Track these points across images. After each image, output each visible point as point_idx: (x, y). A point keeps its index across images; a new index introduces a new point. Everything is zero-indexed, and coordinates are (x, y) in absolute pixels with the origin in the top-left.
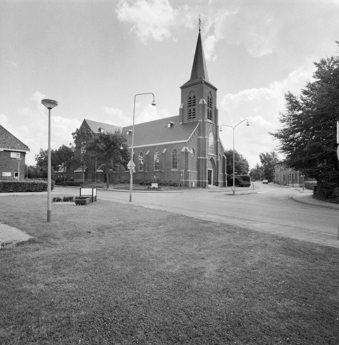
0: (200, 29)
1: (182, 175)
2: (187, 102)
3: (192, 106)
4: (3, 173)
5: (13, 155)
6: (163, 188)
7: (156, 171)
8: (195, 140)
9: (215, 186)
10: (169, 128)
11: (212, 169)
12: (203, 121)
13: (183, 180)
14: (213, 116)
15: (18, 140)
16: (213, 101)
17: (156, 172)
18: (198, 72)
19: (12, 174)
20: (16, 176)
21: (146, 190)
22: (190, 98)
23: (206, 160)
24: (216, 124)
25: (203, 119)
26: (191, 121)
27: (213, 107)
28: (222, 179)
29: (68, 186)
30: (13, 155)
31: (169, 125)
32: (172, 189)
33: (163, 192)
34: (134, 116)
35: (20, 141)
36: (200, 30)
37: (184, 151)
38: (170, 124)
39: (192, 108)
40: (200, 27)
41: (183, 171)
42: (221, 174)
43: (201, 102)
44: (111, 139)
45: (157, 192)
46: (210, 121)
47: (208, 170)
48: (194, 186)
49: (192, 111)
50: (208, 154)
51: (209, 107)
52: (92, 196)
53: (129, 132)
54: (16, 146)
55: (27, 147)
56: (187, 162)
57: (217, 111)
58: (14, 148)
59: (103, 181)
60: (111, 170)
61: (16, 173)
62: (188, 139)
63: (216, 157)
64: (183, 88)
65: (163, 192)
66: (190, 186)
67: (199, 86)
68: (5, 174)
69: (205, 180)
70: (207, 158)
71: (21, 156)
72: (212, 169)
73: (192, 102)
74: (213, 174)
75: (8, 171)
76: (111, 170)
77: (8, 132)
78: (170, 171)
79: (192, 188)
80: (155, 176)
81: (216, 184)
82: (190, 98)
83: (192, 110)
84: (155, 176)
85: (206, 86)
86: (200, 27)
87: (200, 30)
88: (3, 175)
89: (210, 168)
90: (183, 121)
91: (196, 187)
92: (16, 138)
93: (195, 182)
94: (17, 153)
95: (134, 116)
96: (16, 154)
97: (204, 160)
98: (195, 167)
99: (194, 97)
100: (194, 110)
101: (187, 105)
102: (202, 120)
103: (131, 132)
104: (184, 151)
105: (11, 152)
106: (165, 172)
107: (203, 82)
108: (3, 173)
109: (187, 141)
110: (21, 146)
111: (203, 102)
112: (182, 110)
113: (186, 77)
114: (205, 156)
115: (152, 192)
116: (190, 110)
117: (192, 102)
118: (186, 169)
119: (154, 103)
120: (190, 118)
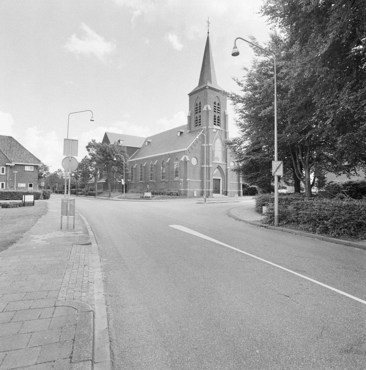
0: (208, 31)
1: (181, 184)
2: (194, 110)
3: (198, 113)
4: (19, 184)
5: (27, 169)
6: (156, 197)
7: (162, 180)
8: (198, 148)
9: (224, 196)
10: (179, 136)
11: (221, 178)
12: (207, 127)
13: (182, 189)
14: (222, 121)
15: (32, 155)
16: (221, 106)
17: (162, 181)
18: (204, 77)
19: (27, 185)
20: (30, 187)
21: (139, 199)
22: (197, 105)
23: (209, 168)
24: (225, 129)
25: (207, 125)
26: (197, 128)
27: (222, 112)
28: (237, 188)
29: (89, 196)
30: (27, 169)
31: (179, 134)
32: (169, 198)
33: (153, 201)
34: (68, 132)
35: (34, 156)
36: (208, 33)
37: (183, 160)
38: (179, 132)
39: (198, 115)
40: (208, 30)
41: (182, 180)
42: (236, 182)
43: (205, 109)
44: (108, 151)
45: (150, 201)
46: (218, 127)
47: (214, 179)
48: (195, 195)
49: (198, 119)
50: (213, 162)
51: (217, 112)
52: (33, 202)
53: (148, 142)
54: (29, 160)
55: (40, 161)
56: (186, 171)
57: (226, 116)
58: (18, 161)
59: (119, 191)
60: (129, 180)
61: (30, 184)
62: (188, 148)
63: (225, 166)
64: (190, 95)
65: (153, 201)
66: (188, 195)
67: (203, 91)
68: (20, 185)
69: (209, 188)
70: (211, 166)
71: (34, 169)
72: (221, 178)
73: (198, 108)
74: (222, 182)
75: (23, 183)
76: (129, 180)
77: (24, 148)
78: (173, 180)
79: (194, 197)
80: (148, 185)
81: (226, 193)
82: (197, 105)
83: (198, 117)
84: (148, 185)
85: (210, 90)
86: (208, 30)
87: (208, 33)
88: (18, 186)
89: (216, 176)
90: (190, 129)
91: (199, 196)
92: (30, 153)
93: (197, 191)
94: (31, 166)
95: (68, 132)
96: (30, 168)
97: (208, 168)
98: (198, 175)
99: (200, 103)
100: (200, 116)
101: (194, 112)
102: (205, 127)
103: (150, 142)
104: (183, 160)
105: (25, 166)
106: (169, 181)
107: (207, 87)
108: (19, 184)
109: (187, 149)
110: (34, 160)
111: (207, 108)
112: (190, 118)
113: (194, 84)
114: (209, 164)
115: (161, 201)
116: (197, 118)
117: (198, 108)
118: (185, 178)
119: (93, 119)
120: (197, 126)
